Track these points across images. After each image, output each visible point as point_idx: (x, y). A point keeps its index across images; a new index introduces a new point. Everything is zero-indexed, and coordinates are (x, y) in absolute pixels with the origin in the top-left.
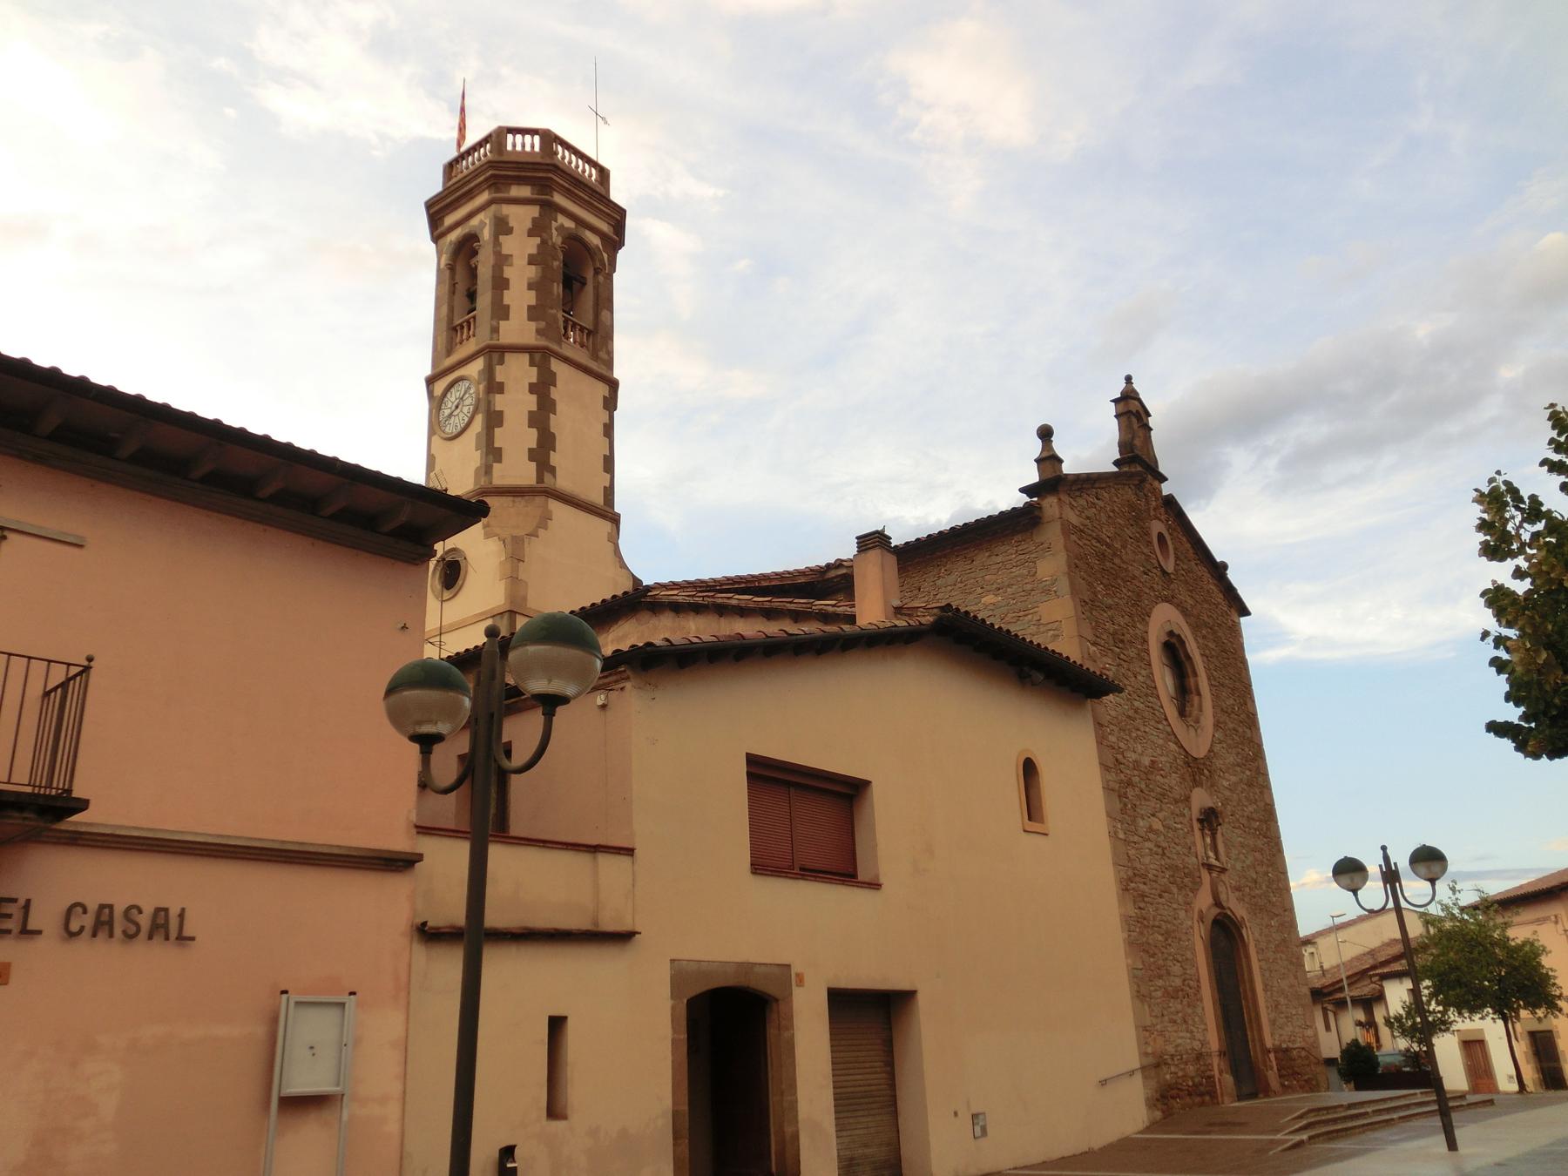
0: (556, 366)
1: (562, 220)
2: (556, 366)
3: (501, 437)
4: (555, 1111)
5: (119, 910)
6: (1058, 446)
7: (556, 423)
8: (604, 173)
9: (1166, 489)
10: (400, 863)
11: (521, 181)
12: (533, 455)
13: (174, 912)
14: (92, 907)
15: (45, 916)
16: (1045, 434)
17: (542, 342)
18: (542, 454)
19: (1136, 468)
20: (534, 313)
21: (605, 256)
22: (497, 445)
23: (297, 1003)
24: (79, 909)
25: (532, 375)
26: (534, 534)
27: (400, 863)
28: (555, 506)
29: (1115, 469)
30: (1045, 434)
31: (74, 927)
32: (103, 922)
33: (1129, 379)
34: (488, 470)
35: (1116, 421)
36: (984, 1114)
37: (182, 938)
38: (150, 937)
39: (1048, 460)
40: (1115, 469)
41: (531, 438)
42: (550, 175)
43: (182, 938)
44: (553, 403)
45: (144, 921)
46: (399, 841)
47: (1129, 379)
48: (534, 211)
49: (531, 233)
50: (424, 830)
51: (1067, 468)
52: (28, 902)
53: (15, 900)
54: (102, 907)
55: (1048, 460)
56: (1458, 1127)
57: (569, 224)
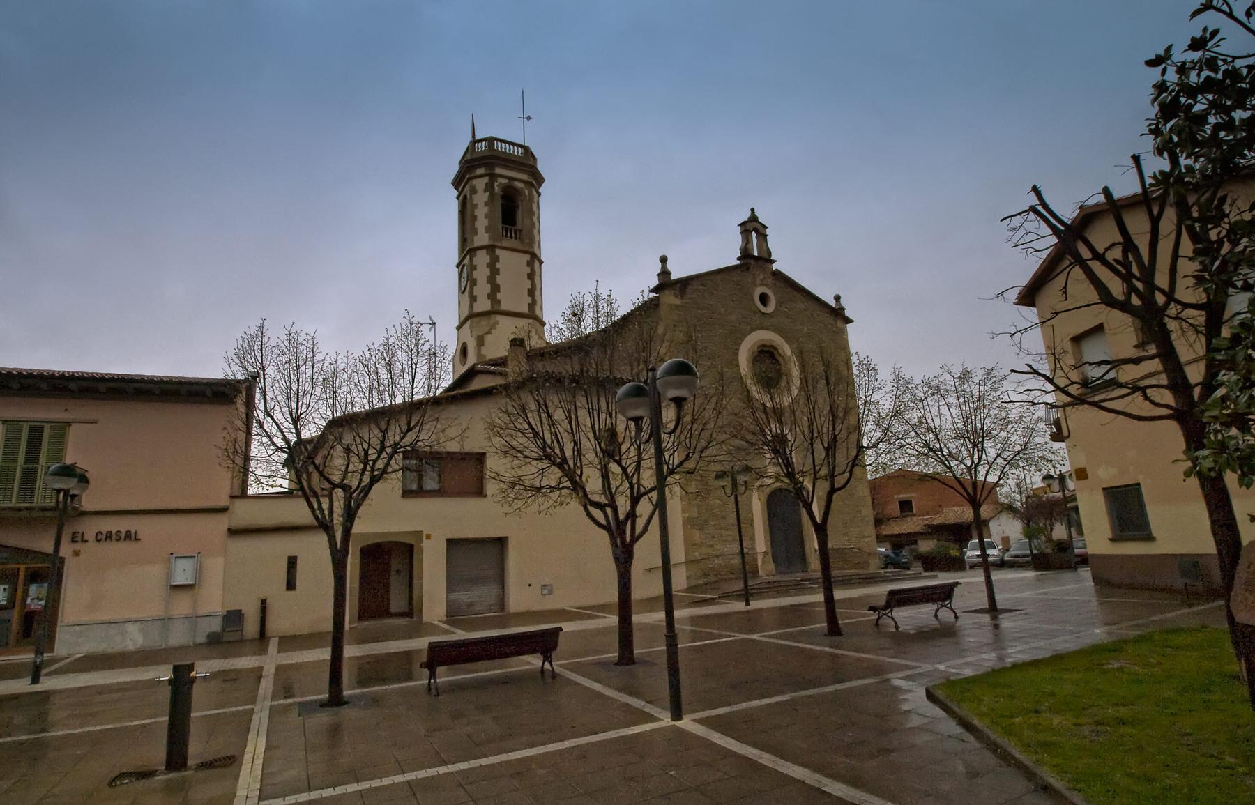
0: (498, 252)
1: (501, 180)
2: (498, 252)
3: (476, 290)
4: (291, 585)
5: (113, 533)
6: (670, 266)
7: (499, 279)
8: (526, 149)
9: (775, 267)
10: (223, 510)
11: (480, 166)
12: (489, 296)
13: (133, 531)
14: (104, 533)
15: (90, 536)
16: (664, 260)
17: (491, 243)
18: (493, 296)
19: (1242, 134)
20: (487, 230)
21: (527, 192)
22: (474, 294)
23: (176, 557)
24: (118, 533)
25: (487, 259)
26: (489, 332)
27: (223, 510)
28: (499, 318)
29: (738, 262)
30: (664, 260)
31: (99, 538)
32: (109, 536)
33: (753, 210)
34: (471, 306)
35: (740, 235)
36: (552, 585)
37: (137, 540)
38: (125, 540)
39: (664, 273)
40: (738, 262)
41: (488, 288)
42: (491, 160)
43: (137, 540)
44: (498, 270)
45: (123, 535)
46: (223, 501)
47: (753, 210)
48: (486, 180)
49: (485, 191)
50: (232, 497)
51: (673, 277)
52: (83, 533)
53: (78, 532)
54: (108, 532)
55: (664, 273)
56: (661, 621)
57: (504, 181)
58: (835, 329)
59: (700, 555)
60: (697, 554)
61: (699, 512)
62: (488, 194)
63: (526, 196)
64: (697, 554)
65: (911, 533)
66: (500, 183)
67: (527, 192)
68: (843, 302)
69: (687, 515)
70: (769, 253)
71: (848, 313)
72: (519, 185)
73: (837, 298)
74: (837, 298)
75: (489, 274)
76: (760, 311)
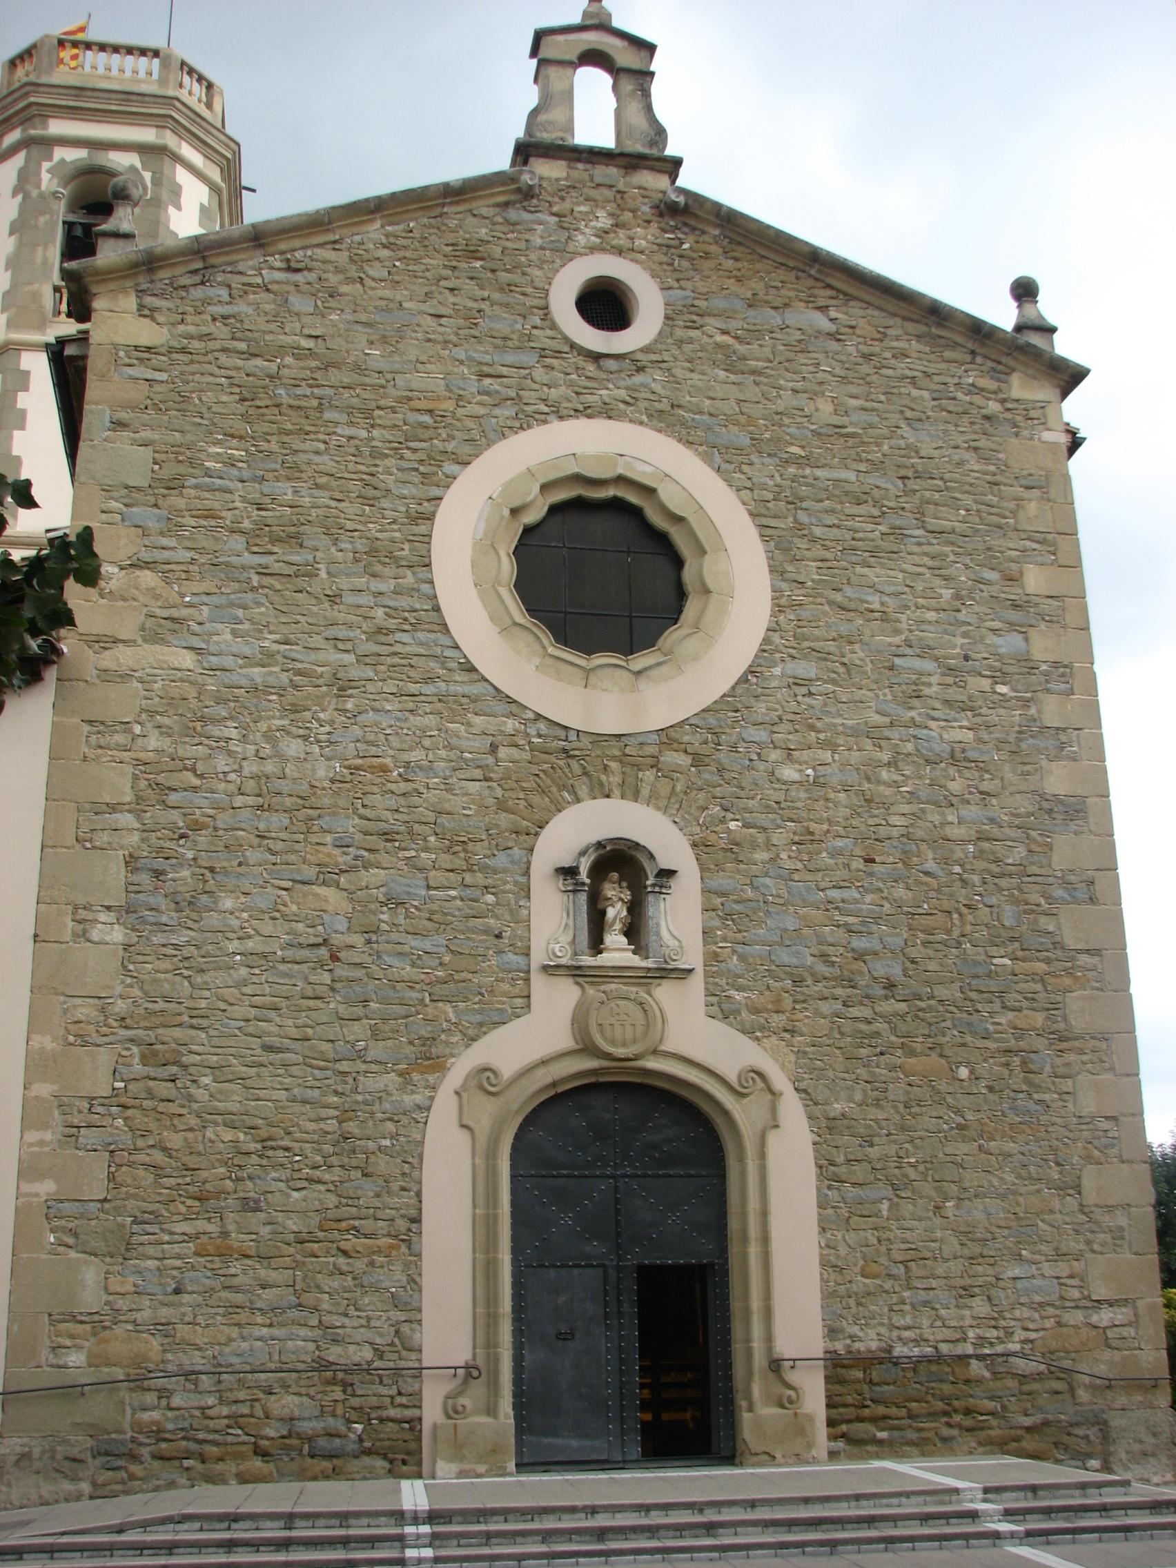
21: (147, 176)
57: (80, 154)
58: (993, 407)
59: (95, 1361)
60: (75, 1359)
61: (111, 1177)
62: (20, 198)
63: (145, 188)
64: (75, 1359)
65: (514, 1404)
66: (63, 162)
67: (147, 176)
68: (1047, 307)
69: (46, 1187)
70: (659, 134)
71: (1065, 347)
72: (121, 160)
73: (1024, 291)
74: (1024, 291)
75: (17, 434)
76: (573, 346)
